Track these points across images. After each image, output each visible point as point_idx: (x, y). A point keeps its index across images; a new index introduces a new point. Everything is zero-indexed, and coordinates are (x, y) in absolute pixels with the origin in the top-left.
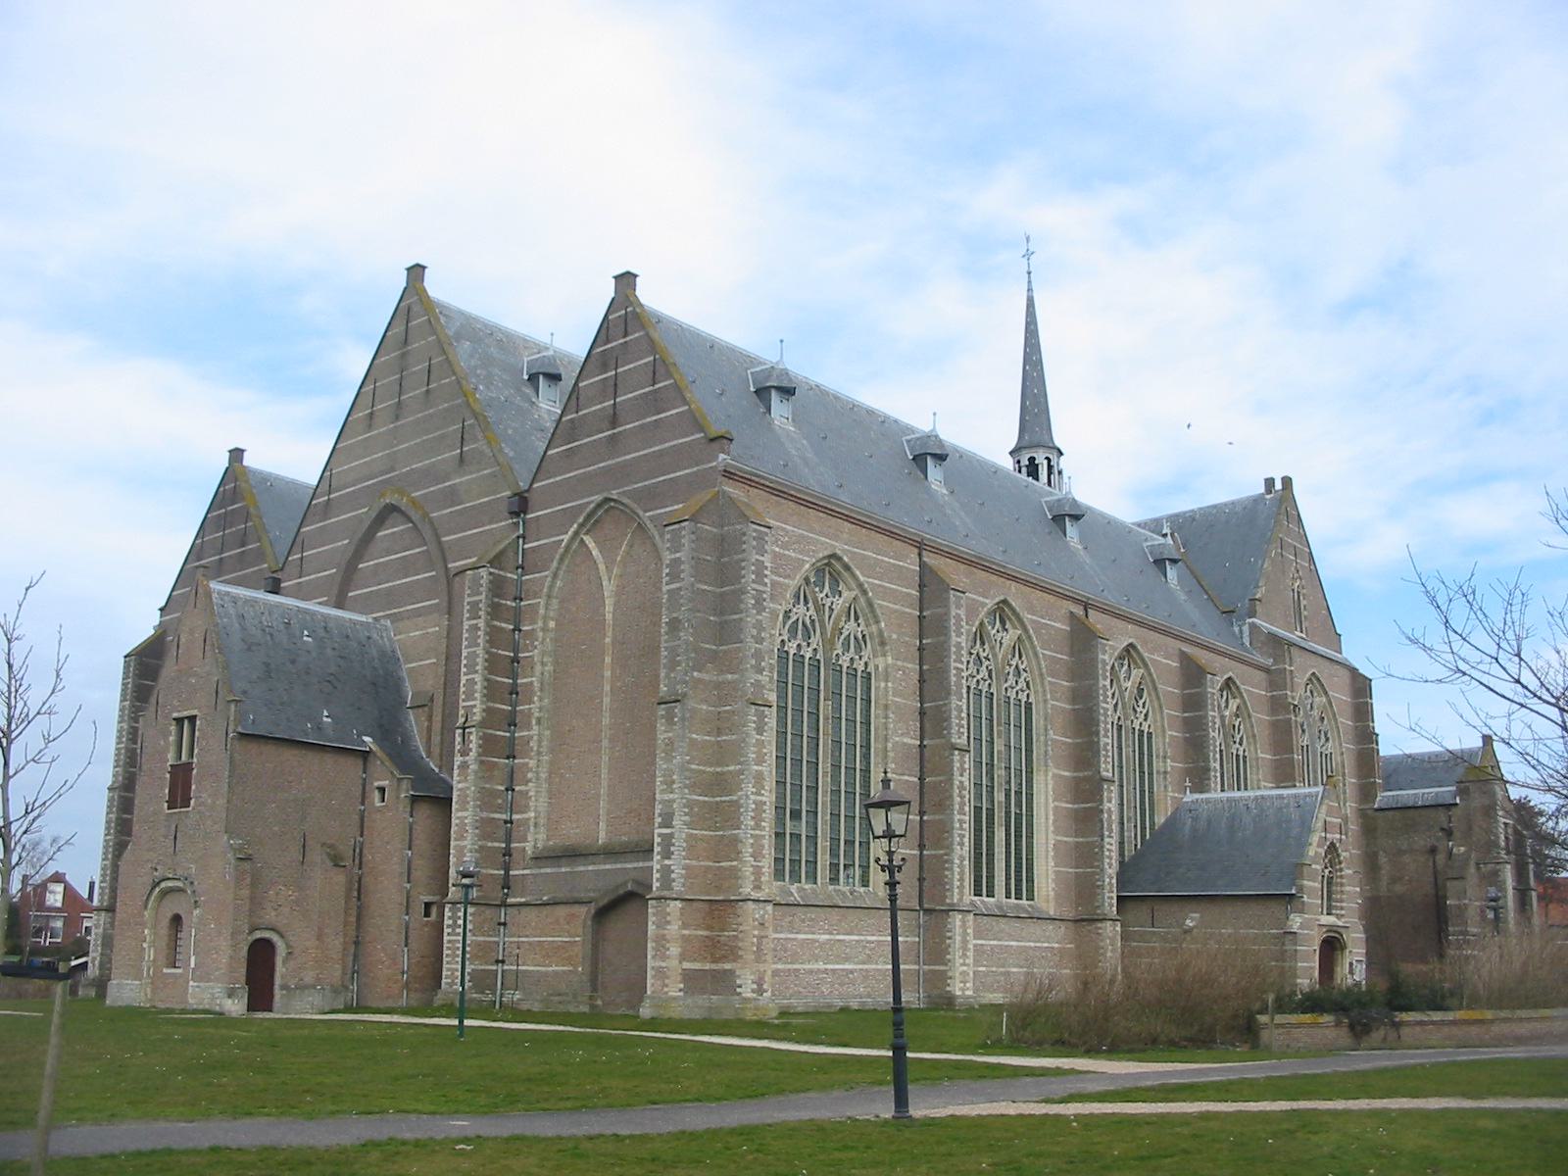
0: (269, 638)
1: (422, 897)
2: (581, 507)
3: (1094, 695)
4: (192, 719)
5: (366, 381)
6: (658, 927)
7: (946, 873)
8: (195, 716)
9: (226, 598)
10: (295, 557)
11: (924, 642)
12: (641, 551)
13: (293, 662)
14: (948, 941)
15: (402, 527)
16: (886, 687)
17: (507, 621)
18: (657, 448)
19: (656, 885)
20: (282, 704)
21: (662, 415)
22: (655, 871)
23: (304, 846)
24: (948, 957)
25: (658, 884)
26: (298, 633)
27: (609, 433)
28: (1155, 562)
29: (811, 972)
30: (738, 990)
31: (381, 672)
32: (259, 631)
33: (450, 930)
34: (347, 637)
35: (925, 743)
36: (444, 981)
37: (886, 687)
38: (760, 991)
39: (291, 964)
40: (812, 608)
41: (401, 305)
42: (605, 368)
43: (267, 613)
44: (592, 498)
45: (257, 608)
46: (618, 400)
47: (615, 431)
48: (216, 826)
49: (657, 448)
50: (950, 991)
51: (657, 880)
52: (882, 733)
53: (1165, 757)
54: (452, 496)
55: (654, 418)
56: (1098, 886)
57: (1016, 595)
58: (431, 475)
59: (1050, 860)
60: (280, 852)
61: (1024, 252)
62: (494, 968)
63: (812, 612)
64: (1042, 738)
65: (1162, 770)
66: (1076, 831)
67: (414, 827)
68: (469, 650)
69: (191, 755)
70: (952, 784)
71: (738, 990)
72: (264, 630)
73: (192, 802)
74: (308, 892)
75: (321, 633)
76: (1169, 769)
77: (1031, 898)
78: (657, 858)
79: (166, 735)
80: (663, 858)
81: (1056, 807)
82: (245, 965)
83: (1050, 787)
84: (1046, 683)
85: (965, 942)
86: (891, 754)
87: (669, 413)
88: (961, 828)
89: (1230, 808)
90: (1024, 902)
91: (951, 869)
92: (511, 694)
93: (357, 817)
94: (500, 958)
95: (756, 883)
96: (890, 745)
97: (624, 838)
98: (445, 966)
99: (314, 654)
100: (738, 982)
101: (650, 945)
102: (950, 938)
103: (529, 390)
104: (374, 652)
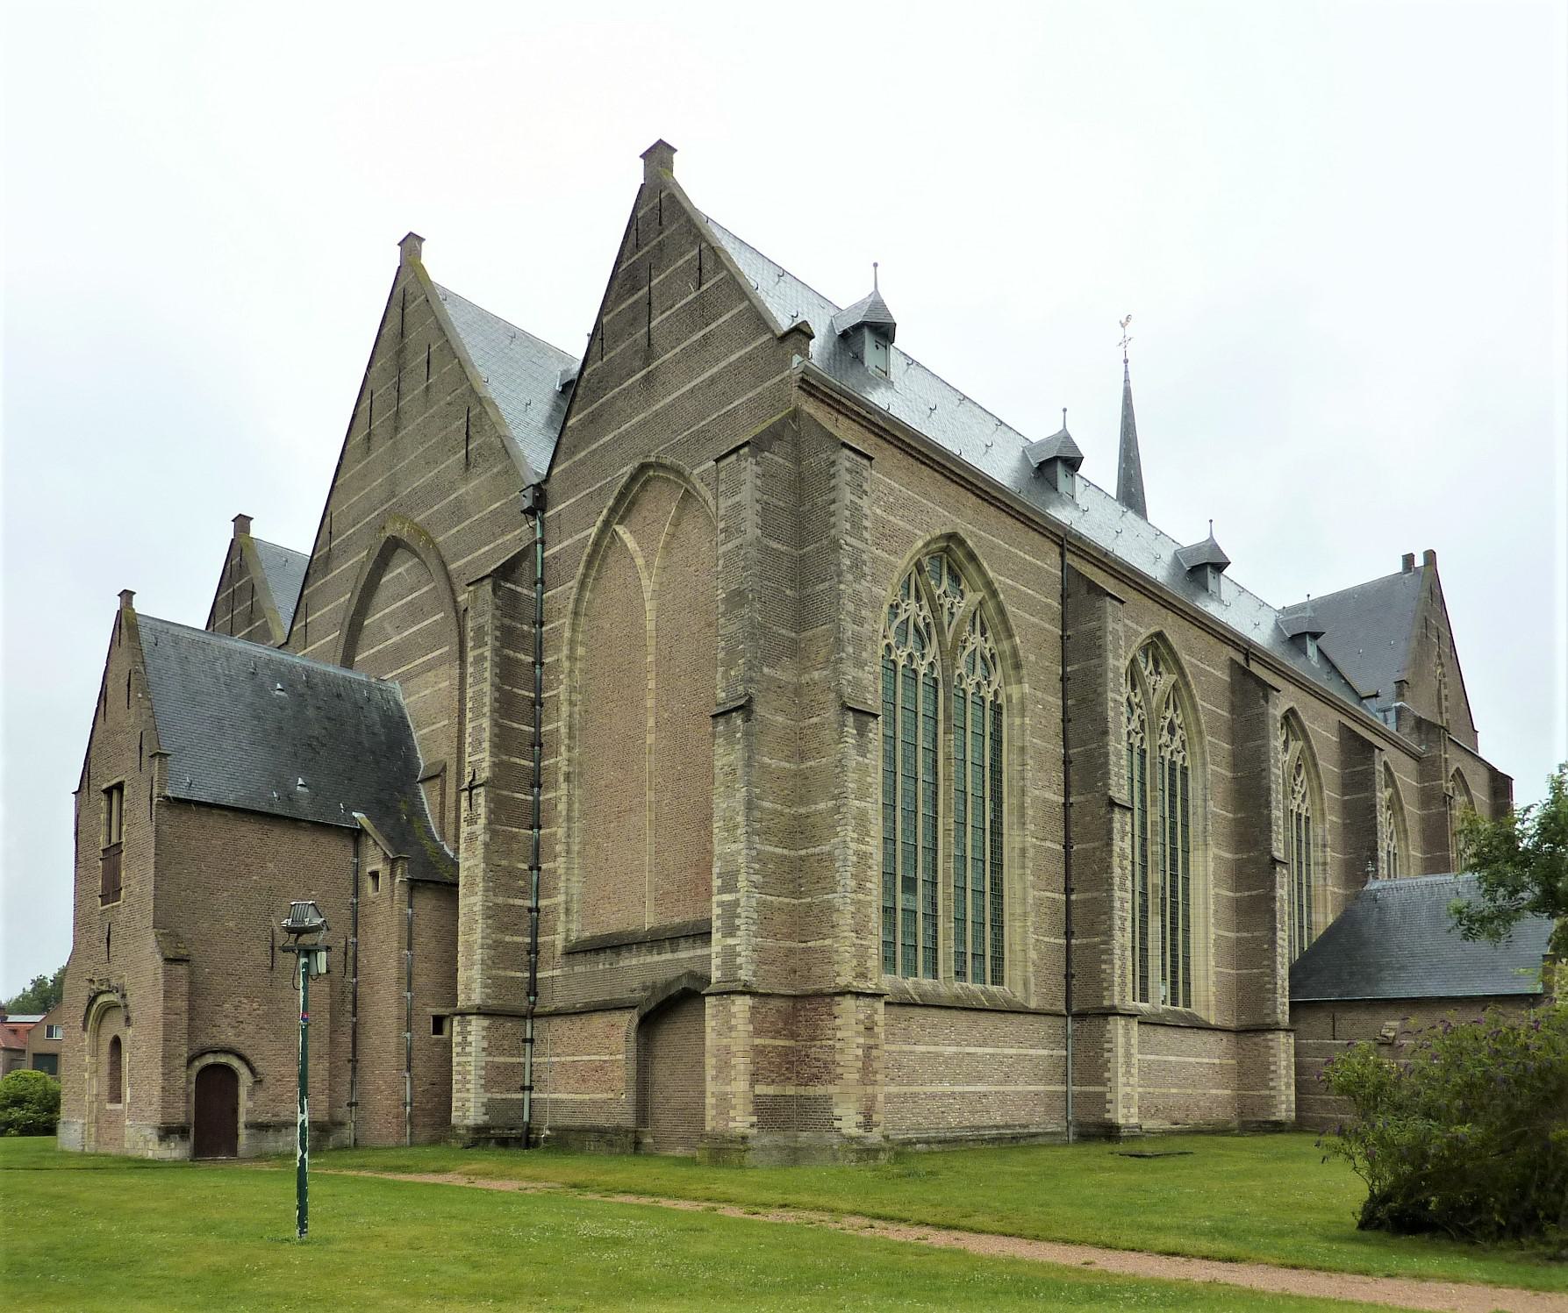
7: (1103, 967)
14: (1106, 1055)
29: (933, 1096)
34: (339, 696)
36: (453, 1114)
53: (1324, 846)
54: (458, 512)
58: (437, 490)
62: (520, 1096)
63: (926, 612)
64: (1200, 810)
65: (1321, 860)
68: (477, 688)
81: (1217, 895)
85: (1128, 1055)
86: (1030, 812)
91: (1111, 962)
96: (1028, 800)
98: (455, 1095)
102: (1110, 1050)
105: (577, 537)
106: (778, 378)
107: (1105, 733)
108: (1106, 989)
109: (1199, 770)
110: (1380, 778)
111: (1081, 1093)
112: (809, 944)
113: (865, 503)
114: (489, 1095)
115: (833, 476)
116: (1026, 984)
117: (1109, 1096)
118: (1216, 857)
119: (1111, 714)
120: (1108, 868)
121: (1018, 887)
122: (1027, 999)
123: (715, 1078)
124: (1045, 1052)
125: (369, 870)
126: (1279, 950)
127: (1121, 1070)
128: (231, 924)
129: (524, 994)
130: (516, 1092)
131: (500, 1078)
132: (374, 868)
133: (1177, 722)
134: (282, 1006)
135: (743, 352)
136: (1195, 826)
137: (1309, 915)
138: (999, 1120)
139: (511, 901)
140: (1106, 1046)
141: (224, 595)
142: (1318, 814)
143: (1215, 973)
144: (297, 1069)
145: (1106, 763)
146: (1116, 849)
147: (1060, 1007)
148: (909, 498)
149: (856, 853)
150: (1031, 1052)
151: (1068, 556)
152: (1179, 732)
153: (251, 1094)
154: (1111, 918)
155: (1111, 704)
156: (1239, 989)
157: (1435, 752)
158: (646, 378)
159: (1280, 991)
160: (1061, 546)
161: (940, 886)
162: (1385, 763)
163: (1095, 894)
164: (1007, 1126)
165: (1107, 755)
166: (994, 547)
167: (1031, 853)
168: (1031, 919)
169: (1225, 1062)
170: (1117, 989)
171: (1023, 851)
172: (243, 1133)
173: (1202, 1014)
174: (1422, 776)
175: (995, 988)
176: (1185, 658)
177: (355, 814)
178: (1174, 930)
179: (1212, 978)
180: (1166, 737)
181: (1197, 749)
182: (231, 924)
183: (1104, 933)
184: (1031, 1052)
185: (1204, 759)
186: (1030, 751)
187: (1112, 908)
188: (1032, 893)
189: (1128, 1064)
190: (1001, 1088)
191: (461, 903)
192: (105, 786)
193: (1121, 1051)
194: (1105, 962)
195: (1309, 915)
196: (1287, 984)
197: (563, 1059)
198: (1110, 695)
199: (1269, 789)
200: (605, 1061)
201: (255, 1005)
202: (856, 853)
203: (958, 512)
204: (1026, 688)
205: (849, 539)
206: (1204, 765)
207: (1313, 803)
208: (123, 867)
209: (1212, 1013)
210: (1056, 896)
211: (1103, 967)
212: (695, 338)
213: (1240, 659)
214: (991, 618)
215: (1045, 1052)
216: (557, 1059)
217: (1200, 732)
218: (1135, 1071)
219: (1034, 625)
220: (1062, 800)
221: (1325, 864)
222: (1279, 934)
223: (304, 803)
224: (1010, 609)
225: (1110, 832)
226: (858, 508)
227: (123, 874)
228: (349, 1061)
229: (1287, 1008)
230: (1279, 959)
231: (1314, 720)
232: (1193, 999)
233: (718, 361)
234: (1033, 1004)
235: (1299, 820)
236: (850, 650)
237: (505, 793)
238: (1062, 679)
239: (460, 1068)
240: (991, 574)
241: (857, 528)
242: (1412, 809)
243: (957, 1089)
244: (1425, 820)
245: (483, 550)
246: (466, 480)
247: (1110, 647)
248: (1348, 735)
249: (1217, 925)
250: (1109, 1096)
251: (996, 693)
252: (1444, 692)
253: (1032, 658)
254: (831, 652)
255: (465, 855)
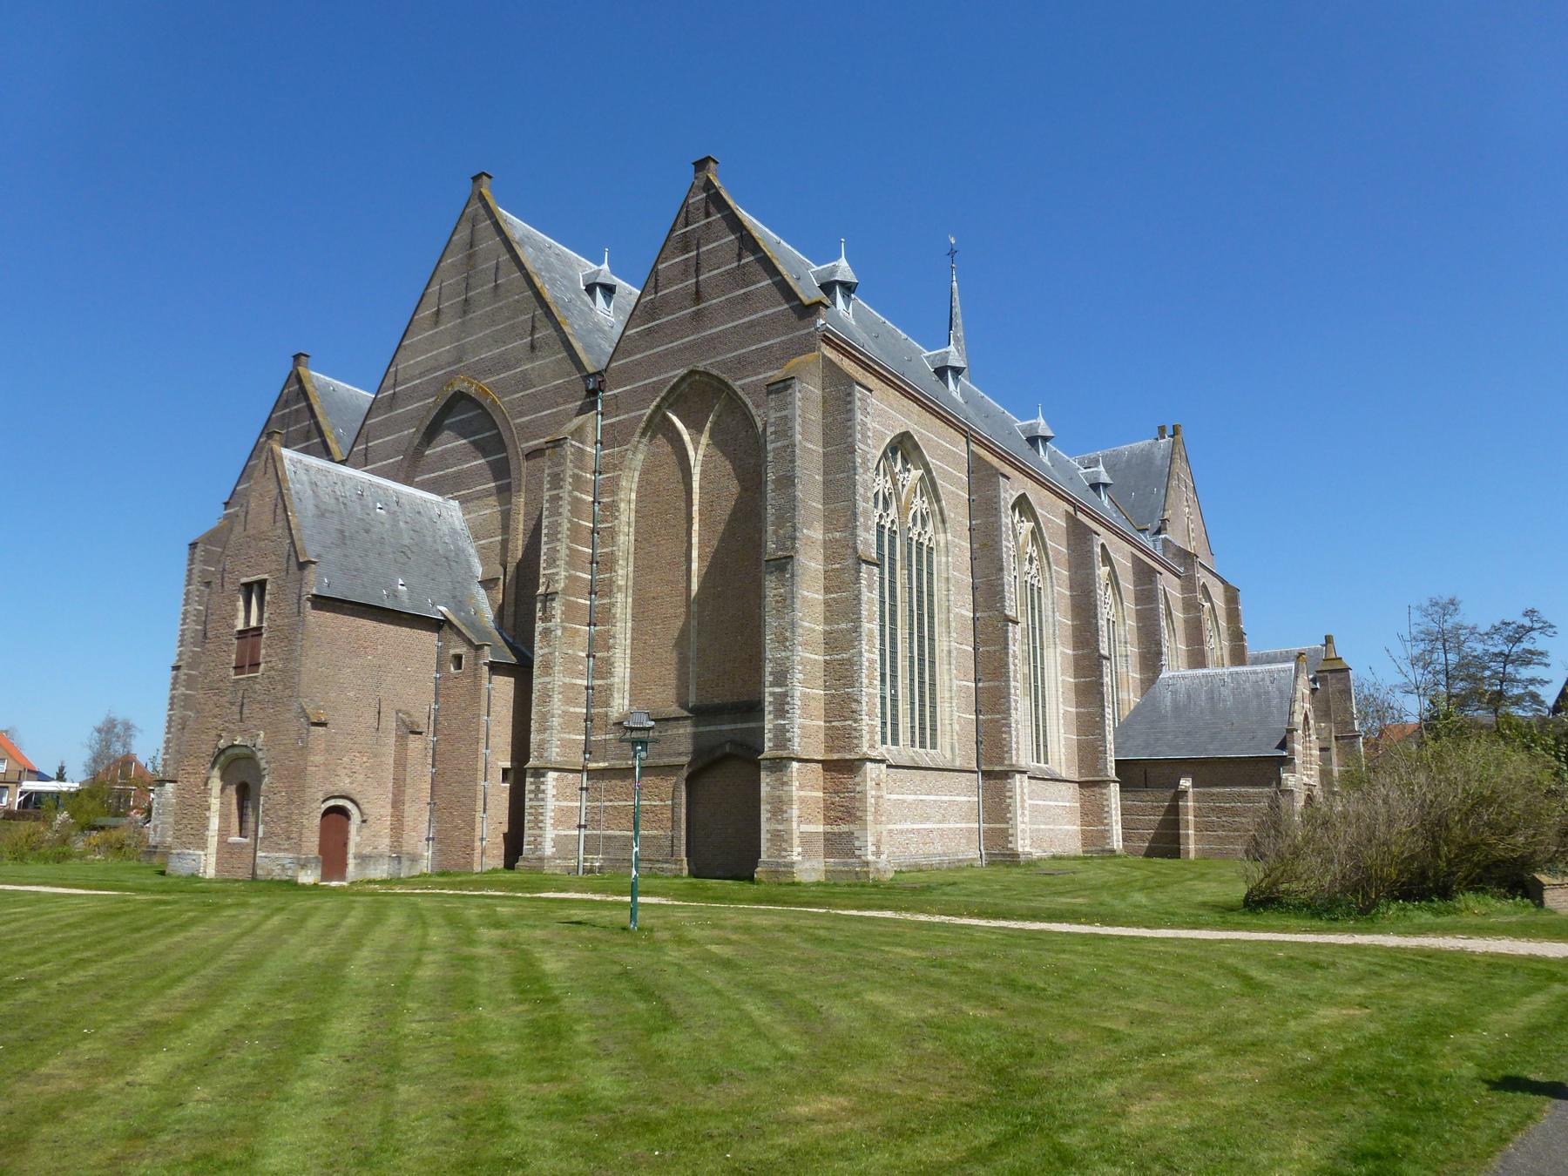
0: (342, 506)
1: (500, 763)
2: (664, 382)
3: (1091, 582)
4: (262, 584)
5: (422, 305)
6: (773, 788)
7: (1004, 736)
8: (265, 580)
9: (299, 465)
10: (361, 447)
11: (974, 522)
12: (729, 420)
13: (367, 531)
14: (1008, 800)
15: (471, 414)
16: (947, 562)
17: (587, 493)
18: (746, 319)
19: (768, 745)
20: (356, 570)
21: (753, 288)
22: (766, 731)
23: (379, 713)
24: (1008, 815)
25: (771, 744)
26: (371, 505)
27: (693, 309)
28: (1090, 486)
29: (902, 832)
30: (857, 852)
31: (452, 547)
32: (333, 501)
33: (532, 796)
34: (419, 513)
35: (978, 615)
36: (525, 847)
37: (947, 562)
38: (878, 853)
39: (366, 832)
40: (890, 481)
41: (467, 211)
42: (686, 250)
43: (340, 483)
44: (676, 372)
45: (330, 478)
46: (701, 278)
47: (699, 307)
48: (287, 691)
49: (746, 319)
50: (1012, 849)
51: (770, 740)
52: (944, 604)
53: (1126, 643)
54: (524, 381)
55: (742, 291)
56: (1100, 752)
57: (1036, 494)
58: (504, 363)
59: (1061, 727)
60: (354, 719)
61: (956, 256)
62: (577, 832)
63: (889, 485)
64: (1050, 619)
65: (1124, 653)
66: (1077, 702)
67: (492, 692)
68: (551, 519)
69: (260, 619)
70: (1007, 654)
71: (857, 852)
72: (337, 499)
73: (262, 666)
74: (383, 759)
75: (394, 507)
76: (1129, 653)
77: (1046, 763)
78: (768, 717)
79: (233, 603)
80: (776, 718)
81: (1063, 680)
82: (318, 834)
83: (1059, 662)
84: (1053, 571)
85: (1023, 801)
86: (953, 624)
87: (759, 285)
88: (1016, 695)
89: (1207, 683)
90: (1042, 765)
91: (1010, 733)
92: (592, 563)
93: (871, 387)
94: (583, 823)
95: (872, 742)
96: (952, 615)
97: (716, 701)
98: (527, 832)
99: (387, 526)
100: (857, 844)
101: (764, 807)
102: (1010, 797)
103: (587, 298)
104: (445, 529)
105: (633, 414)
106: (806, 331)
107: (1001, 569)
108: (1007, 752)
109: (1049, 590)
110: (1098, 559)
111: (990, 829)
112: (833, 724)
113: (868, 420)
114: (556, 832)
115: (850, 402)
116: (952, 749)
117: (1010, 831)
118: (1062, 653)
119: (1005, 556)
120: (1007, 664)
121: (946, 678)
122: (953, 760)
123: (769, 819)
124: (966, 799)
125: (452, 652)
126: (1107, 722)
127: (1019, 812)
128: (351, 694)
129: (581, 753)
130: (574, 829)
131: (563, 819)
132: (458, 651)
133: (1034, 555)
134: (383, 759)
135: (776, 310)
136: (1048, 631)
137: (1117, 694)
138: (940, 849)
139: (574, 681)
140: (1008, 794)
141: (280, 413)
142: (1121, 620)
143: (1065, 738)
144: (362, 807)
145: (1003, 591)
146: (1011, 651)
147: (973, 766)
148: (882, 409)
149: (868, 660)
150: (957, 798)
151: (971, 444)
152: (1035, 562)
153: (359, 830)
154: (1009, 702)
155: (1004, 549)
156: (1079, 750)
157: (1191, 573)
158: (696, 313)
159: (1108, 752)
160: (966, 437)
161: (900, 678)
162: (1103, 546)
163: (997, 684)
164: (945, 854)
165: (1003, 585)
166: (930, 440)
167: (954, 654)
168: (955, 701)
169: (1073, 804)
170: (1014, 752)
171: (949, 652)
172: (351, 862)
173: (1057, 770)
174: (1184, 589)
175: (933, 751)
176: (1039, 511)
177: (439, 607)
178: (1037, 706)
179: (1062, 742)
180: (1027, 567)
181: (1047, 575)
182: (351, 694)
183: (1004, 712)
184: (957, 798)
185: (1052, 582)
186: (952, 581)
187: (1009, 694)
188: (955, 682)
189: (1023, 808)
190: (940, 826)
191: (535, 681)
192: (244, 580)
193: (1018, 797)
194: (1005, 732)
195: (1117, 694)
196: (1112, 747)
197: (616, 804)
198: (1004, 543)
199: (1096, 606)
200: (655, 806)
201: (365, 759)
202: (868, 660)
203: (908, 417)
204: (949, 537)
205: (859, 444)
206: (1052, 586)
207: (1117, 612)
208: (262, 646)
209: (1064, 767)
210: (969, 684)
211: (1004, 736)
212: (738, 293)
213: (1071, 510)
214: (929, 486)
215: (966, 799)
216: (611, 804)
217: (1049, 563)
218: (1026, 812)
219: (953, 492)
220: (972, 615)
221: (1127, 656)
222: (1107, 710)
223: (405, 598)
224: (939, 482)
225: (1006, 638)
226: (864, 424)
227: (263, 652)
228: (428, 804)
229: (1113, 765)
230: (1107, 728)
231: (1116, 551)
232: (1049, 758)
233: (756, 312)
234: (958, 764)
235: (1032, 590)
236: (862, 520)
237: (572, 598)
238: (970, 530)
239: (533, 811)
240: (928, 458)
241: (865, 436)
242: (1178, 615)
243: (915, 826)
244: (1186, 621)
245: (545, 413)
246: (532, 360)
247: (1003, 510)
248: (1137, 561)
249: (1064, 703)
250: (1010, 831)
251: (930, 539)
252: (1191, 526)
253: (952, 515)
254: (849, 521)
255: (540, 645)
